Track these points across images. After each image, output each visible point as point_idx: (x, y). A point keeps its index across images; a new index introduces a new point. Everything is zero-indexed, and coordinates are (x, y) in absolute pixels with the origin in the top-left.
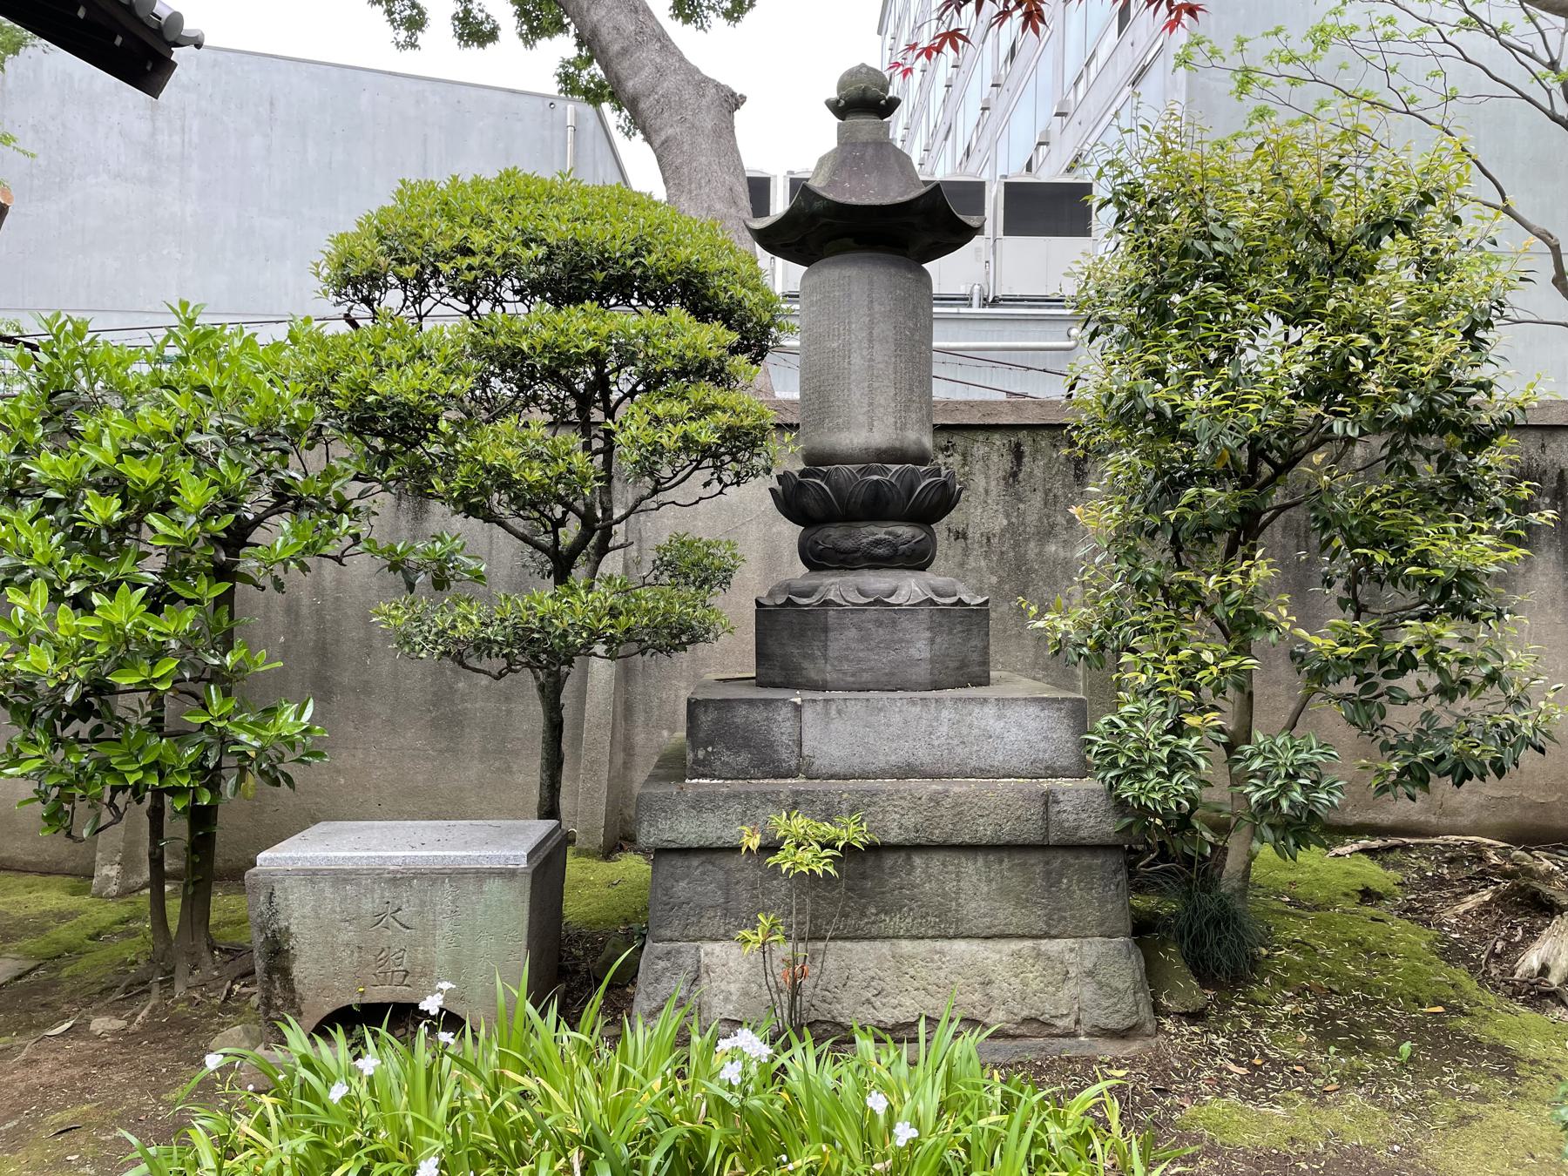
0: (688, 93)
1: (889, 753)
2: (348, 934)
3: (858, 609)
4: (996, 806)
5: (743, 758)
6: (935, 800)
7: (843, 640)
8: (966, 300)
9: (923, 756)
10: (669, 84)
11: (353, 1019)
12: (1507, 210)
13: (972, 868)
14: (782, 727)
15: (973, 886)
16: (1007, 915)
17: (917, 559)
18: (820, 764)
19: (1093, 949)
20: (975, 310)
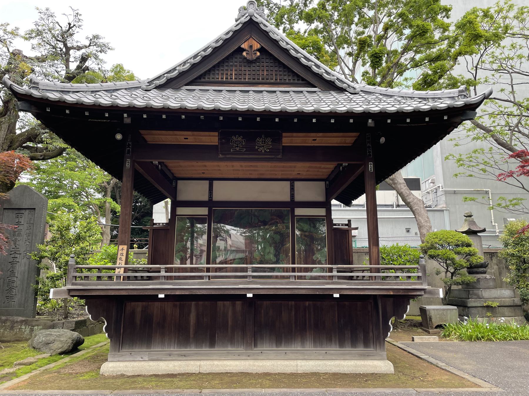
0: (418, 202)
1: (494, 296)
2: (438, 316)
3: (483, 279)
4: (508, 302)
5: (476, 297)
6: (501, 301)
7: (482, 283)
8: (392, 206)
9: (497, 296)
10: (415, 201)
11: (437, 327)
12: (523, 188)
13: (505, 308)
14: (480, 293)
15: (506, 310)
16: (510, 314)
17: (485, 273)
18: (485, 297)
19: (520, 318)
20: (395, 208)
